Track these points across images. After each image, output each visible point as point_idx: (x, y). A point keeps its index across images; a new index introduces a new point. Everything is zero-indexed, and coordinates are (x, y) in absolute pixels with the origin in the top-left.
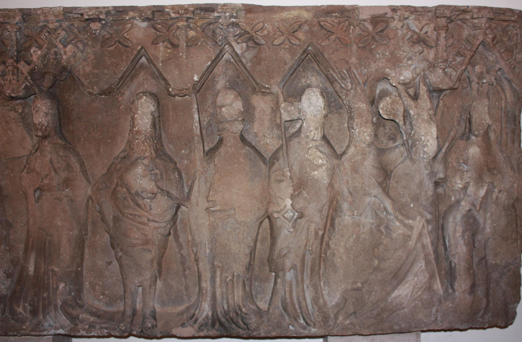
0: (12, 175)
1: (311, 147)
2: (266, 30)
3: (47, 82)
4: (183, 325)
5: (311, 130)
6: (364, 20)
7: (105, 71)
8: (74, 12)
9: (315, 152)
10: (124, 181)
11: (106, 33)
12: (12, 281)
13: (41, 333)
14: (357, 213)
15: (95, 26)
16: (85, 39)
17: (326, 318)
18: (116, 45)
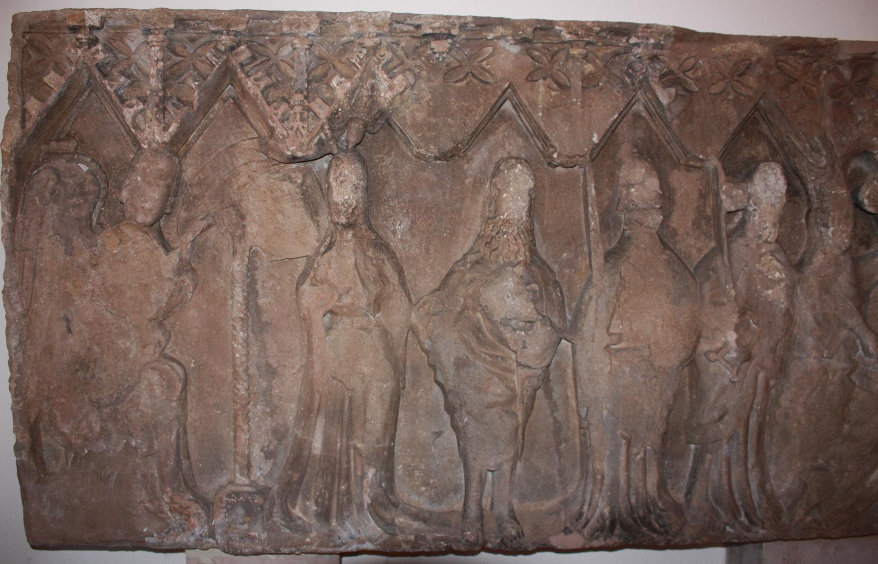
0: (278, 288)
1: (765, 253)
2: (700, 70)
3: (351, 136)
4: (567, 531)
5: (766, 228)
6: (841, 63)
7: (449, 120)
8: (409, 21)
9: (771, 260)
10: (481, 301)
11: (452, 59)
12: (274, 464)
13: (337, 549)
14: (828, 354)
15: (439, 46)
16: (415, 66)
17: (777, 512)
18: (468, 79)
